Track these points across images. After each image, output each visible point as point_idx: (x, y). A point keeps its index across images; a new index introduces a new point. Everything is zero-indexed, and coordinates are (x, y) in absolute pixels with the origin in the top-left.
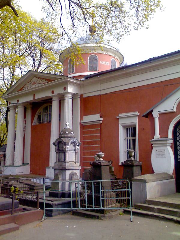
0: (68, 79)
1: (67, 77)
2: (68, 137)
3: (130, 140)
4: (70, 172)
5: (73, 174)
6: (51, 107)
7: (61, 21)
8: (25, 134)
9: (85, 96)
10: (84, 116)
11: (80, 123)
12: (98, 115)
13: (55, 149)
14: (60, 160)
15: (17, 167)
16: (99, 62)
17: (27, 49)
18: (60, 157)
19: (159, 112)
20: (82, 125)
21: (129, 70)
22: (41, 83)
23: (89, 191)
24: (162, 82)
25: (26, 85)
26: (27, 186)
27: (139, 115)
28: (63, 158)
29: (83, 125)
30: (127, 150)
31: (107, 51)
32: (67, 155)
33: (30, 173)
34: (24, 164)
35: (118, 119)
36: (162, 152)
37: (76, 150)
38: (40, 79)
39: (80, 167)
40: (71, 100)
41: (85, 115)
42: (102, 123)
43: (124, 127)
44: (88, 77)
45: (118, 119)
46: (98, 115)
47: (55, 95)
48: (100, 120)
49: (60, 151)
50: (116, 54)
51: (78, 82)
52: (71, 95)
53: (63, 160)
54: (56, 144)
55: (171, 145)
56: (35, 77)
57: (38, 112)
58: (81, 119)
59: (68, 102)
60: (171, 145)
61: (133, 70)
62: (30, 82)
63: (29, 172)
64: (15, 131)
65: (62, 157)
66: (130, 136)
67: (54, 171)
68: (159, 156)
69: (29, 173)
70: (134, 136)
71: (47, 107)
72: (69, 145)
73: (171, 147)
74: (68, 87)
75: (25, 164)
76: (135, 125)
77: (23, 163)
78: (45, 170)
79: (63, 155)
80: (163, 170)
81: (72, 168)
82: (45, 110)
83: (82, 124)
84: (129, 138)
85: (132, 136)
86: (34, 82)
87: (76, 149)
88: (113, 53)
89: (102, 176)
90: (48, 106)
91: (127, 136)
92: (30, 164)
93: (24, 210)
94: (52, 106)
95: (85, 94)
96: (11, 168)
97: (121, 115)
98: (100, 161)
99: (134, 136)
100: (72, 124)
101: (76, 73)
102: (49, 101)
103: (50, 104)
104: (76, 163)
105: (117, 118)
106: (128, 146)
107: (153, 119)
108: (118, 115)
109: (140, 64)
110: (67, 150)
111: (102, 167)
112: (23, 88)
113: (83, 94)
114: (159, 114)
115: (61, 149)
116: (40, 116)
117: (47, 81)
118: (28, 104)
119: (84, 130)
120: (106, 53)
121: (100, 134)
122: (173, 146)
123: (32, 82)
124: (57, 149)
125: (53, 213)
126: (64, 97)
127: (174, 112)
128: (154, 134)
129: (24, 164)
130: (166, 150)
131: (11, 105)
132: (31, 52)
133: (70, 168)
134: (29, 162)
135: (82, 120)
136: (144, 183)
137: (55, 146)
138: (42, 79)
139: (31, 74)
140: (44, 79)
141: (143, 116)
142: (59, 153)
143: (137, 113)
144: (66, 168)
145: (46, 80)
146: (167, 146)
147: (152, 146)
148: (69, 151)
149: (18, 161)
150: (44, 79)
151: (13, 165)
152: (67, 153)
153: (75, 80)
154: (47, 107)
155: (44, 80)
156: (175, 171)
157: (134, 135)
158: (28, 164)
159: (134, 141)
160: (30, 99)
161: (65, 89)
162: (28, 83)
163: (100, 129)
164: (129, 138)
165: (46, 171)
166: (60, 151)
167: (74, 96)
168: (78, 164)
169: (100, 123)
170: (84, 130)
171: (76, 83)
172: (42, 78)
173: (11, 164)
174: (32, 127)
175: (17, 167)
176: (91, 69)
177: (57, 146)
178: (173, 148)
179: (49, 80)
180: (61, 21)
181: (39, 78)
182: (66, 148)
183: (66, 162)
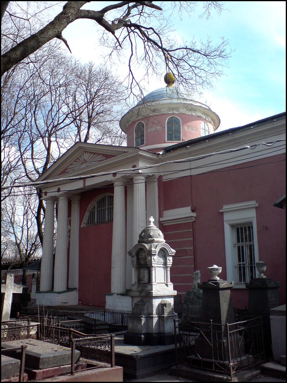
0: (139, 153)
1: (137, 149)
3: (242, 247)
6: (112, 198)
7: (129, 66)
8: (69, 242)
9: (165, 179)
10: (164, 211)
13: (132, 261)
14: (142, 281)
15: (59, 293)
16: (183, 127)
17: (68, 114)
18: (142, 275)
20: (162, 224)
21: (237, 135)
23: (99, 339)
25: (71, 164)
26: (82, 324)
27: (257, 205)
29: (164, 225)
30: (238, 263)
31: (195, 110)
33: (79, 303)
35: (222, 213)
38: (93, 155)
39: (175, 293)
41: (166, 209)
42: (194, 221)
43: (232, 226)
44: (168, 150)
45: (222, 213)
47: (119, 178)
49: (140, 266)
50: (208, 115)
51: (155, 158)
52: (143, 178)
53: (146, 280)
54: (134, 253)
56: (86, 152)
57: (90, 207)
59: (140, 188)
61: (216, 143)
62: (78, 161)
63: (78, 301)
66: (242, 241)
67: (131, 298)
69: (77, 304)
70: (250, 241)
71: (104, 200)
75: (70, 289)
76: (251, 223)
77: (68, 288)
78: (105, 299)
79: (146, 272)
82: (101, 203)
83: (162, 223)
84: (240, 244)
85: (246, 241)
86: (84, 160)
88: (204, 113)
90: (105, 197)
91: (238, 241)
93: (90, 366)
94: (113, 197)
95: (166, 176)
97: (226, 207)
98: (216, 280)
99: (250, 241)
102: (109, 188)
103: (111, 194)
105: (221, 211)
106: (241, 257)
108: (222, 207)
109: (256, 125)
112: (66, 169)
113: (163, 176)
115: (142, 262)
116: (92, 214)
117: (104, 158)
118: (74, 195)
120: (194, 114)
121: (192, 239)
123: (81, 160)
124: (135, 262)
125: (137, 372)
126: (133, 182)
131: (60, 193)
132: (75, 119)
134: (76, 285)
135: (163, 217)
137: (132, 257)
139: (79, 146)
140: (99, 154)
141: (276, 205)
142: (140, 268)
143: (253, 203)
149: (60, 285)
150: (99, 154)
152: (154, 269)
153: (151, 154)
154: (104, 200)
157: (251, 239)
159: (251, 248)
160: (79, 185)
162: (75, 161)
163: (192, 230)
164: (240, 244)
165: (107, 300)
166: (140, 266)
167: (148, 179)
168: (171, 286)
171: (150, 159)
174: (81, 230)
175: (59, 293)
176: (170, 139)
177: (136, 257)
179: (108, 157)
180: (129, 66)
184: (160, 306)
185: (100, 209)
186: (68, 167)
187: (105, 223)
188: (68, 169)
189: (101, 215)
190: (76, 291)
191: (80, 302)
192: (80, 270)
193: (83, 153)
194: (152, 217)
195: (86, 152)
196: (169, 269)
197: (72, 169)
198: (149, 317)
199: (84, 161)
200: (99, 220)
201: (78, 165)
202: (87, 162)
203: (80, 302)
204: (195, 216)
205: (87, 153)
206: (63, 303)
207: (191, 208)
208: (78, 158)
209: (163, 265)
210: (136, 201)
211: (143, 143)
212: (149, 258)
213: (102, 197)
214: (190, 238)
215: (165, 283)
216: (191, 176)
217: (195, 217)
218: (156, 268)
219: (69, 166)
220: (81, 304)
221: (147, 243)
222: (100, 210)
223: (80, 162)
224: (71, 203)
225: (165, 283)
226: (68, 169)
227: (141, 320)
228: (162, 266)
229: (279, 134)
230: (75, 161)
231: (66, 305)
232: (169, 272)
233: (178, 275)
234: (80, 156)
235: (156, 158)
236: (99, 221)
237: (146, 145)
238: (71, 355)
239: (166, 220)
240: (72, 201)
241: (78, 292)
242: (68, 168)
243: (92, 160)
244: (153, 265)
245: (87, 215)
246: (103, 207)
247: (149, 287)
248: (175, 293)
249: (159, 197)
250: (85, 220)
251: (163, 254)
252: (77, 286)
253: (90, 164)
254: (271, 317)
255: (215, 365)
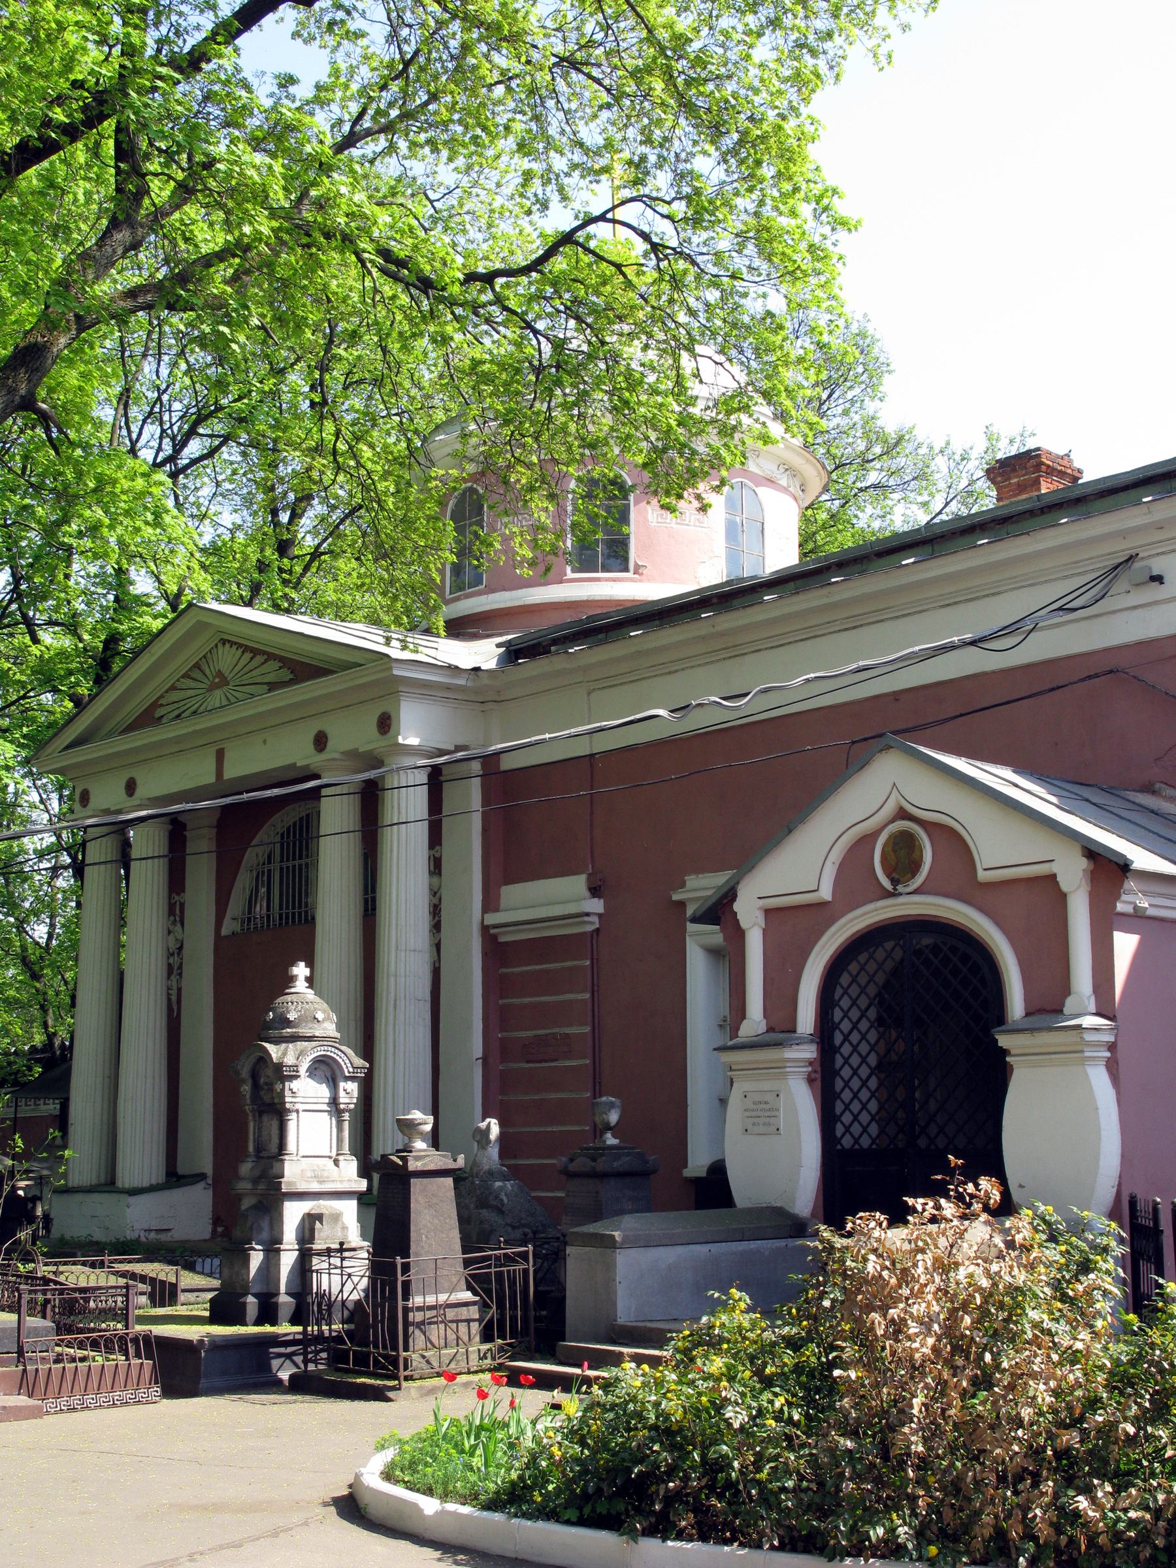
2: (295, 1038)
4: (306, 1206)
5: (319, 1217)
10: (506, 883)
11: (485, 929)
12: (577, 884)
18: (265, 1133)
19: (761, 902)
20: (495, 937)
22: (259, 680)
24: (896, 696)
28: (275, 1140)
29: (502, 939)
32: (292, 1126)
33: (214, 1231)
34: (174, 1178)
36: (766, 1103)
37: (342, 1100)
38: (248, 656)
40: (422, 794)
41: (511, 878)
42: (597, 930)
46: (577, 884)
48: (588, 914)
53: (274, 1149)
55: (810, 1069)
58: (490, 903)
60: (810, 1069)
62: (197, 674)
63: (210, 1228)
64: (122, 974)
65: (270, 1135)
68: (754, 1124)
72: (297, 1077)
73: (810, 1081)
74: (402, 715)
75: (183, 1177)
79: (275, 1124)
80: (770, 1197)
81: (315, 1187)
83: (492, 931)
86: (220, 674)
87: (342, 1093)
89: (413, 1215)
92: (210, 1181)
96: (101, 1203)
100: (436, 927)
101: (493, 591)
104: (341, 1164)
105: (675, 897)
107: (737, 935)
108: (683, 885)
110: (287, 1099)
111: (416, 1184)
112: (155, 705)
114: (768, 912)
119: (505, 970)
121: (587, 996)
122: (818, 1076)
123: (207, 672)
127: (823, 905)
128: (744, 1017)
129: (174, 1178)
130: (781, 1096)
133: (302, 1187)
134: (206, 1165)
135: (497, 910)
136: (608, 1250)
138: (259, 659)
140: (270, 656)
142: (261, 1113)
144: (283, 1186)
145: (285, 662)
146: (784, 1076)
147: (1112, 1039)
148: (300, 1107)
151: (108, 1184)
152: (293, 1116)
155: (274, 665)
156: (821, 1198)
158: (202, 1177)
161: (385, 724)
168: (350, 1166)
169: (589, 928)
170: (505, 970)
172: (264, 653)
173: (103, 1180)
174: (220, 942)
178: (818, 1084)
181: (246, 649)
182: (283, 1090)
183: (286, 1157)
184: (307, 1223)
185: (290, 864)
186: (162, 696)
187: (306, 920)
188: (162, 705)
189: (294, 888)
190: (202, 1185)
191: (220, 1229)
192: (216, 1105)
193: (216, 646)
194: (302, 964)
195: (224, 644)
196: (346, 1116)
197: (176, 705)
198: (273, 1250)
199: (217, 680)
200: (287, 908)
201: (191, 693)
202: (228, 684)
203: (220, 1229)
204: (601, 910)
205: (227, 645)
206: (151, 1230)
207: (588, 879)
208: (197, 666)
209: (328, 1104)
210: (391, 851)
211: (478, 581)
212: (278, 1087)
213: (291, 823)
214: (582, 991)
215: (330, 1157)
216: (592, 756)
217: (600, 916)
218: (301, 1113)
219: (167, 692)
220: (223, 1235)
221: (277, 1041)
222: (288, 868)
223: (206, 681)
224: (185, 837)
225: (330, 1157)
226: (162, 705)
227: (246, 1260)
228: (325, 1107)
229: (855, 628)
230: (186, 676)
231: (164, 1237)
232: (346, 1125)
233: (542, 1129)
234: (204, 657)
235: (470, 684)
236: (291, 910)
237: (491, 590)
238: (16, 1325)
239: (520, 919)
240: (189, 826)
241: (210, 1192)
242: (162, 701)
243: (246, 679)
244: (288, 1106)
245: (243, 882)
246: (288, 860)
247: (276, 1165)
248: (363, 1185)
249: (485, 831)
250: (236, 906)
251: (328, 1075)
252: (207, 1167)
253: (237, 695)
254: (569, 1250)
255: (375, 1360)
